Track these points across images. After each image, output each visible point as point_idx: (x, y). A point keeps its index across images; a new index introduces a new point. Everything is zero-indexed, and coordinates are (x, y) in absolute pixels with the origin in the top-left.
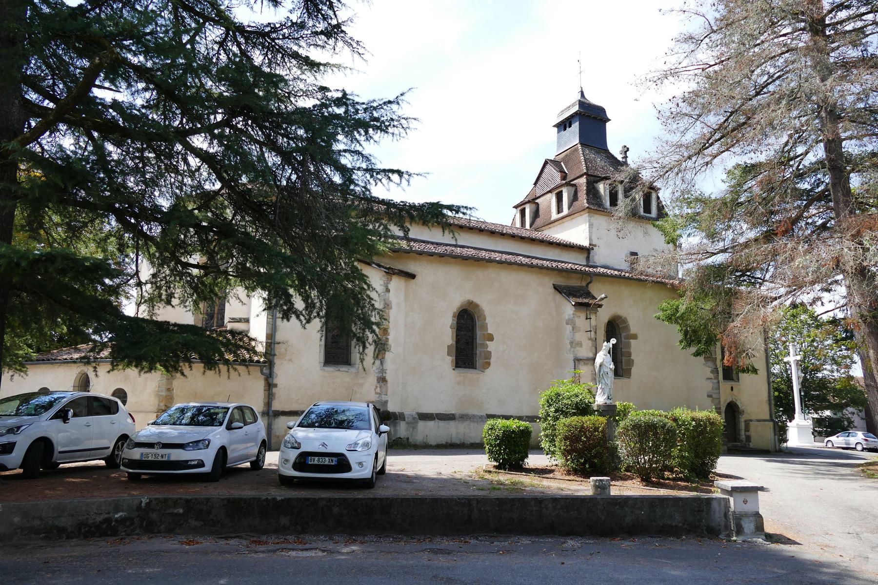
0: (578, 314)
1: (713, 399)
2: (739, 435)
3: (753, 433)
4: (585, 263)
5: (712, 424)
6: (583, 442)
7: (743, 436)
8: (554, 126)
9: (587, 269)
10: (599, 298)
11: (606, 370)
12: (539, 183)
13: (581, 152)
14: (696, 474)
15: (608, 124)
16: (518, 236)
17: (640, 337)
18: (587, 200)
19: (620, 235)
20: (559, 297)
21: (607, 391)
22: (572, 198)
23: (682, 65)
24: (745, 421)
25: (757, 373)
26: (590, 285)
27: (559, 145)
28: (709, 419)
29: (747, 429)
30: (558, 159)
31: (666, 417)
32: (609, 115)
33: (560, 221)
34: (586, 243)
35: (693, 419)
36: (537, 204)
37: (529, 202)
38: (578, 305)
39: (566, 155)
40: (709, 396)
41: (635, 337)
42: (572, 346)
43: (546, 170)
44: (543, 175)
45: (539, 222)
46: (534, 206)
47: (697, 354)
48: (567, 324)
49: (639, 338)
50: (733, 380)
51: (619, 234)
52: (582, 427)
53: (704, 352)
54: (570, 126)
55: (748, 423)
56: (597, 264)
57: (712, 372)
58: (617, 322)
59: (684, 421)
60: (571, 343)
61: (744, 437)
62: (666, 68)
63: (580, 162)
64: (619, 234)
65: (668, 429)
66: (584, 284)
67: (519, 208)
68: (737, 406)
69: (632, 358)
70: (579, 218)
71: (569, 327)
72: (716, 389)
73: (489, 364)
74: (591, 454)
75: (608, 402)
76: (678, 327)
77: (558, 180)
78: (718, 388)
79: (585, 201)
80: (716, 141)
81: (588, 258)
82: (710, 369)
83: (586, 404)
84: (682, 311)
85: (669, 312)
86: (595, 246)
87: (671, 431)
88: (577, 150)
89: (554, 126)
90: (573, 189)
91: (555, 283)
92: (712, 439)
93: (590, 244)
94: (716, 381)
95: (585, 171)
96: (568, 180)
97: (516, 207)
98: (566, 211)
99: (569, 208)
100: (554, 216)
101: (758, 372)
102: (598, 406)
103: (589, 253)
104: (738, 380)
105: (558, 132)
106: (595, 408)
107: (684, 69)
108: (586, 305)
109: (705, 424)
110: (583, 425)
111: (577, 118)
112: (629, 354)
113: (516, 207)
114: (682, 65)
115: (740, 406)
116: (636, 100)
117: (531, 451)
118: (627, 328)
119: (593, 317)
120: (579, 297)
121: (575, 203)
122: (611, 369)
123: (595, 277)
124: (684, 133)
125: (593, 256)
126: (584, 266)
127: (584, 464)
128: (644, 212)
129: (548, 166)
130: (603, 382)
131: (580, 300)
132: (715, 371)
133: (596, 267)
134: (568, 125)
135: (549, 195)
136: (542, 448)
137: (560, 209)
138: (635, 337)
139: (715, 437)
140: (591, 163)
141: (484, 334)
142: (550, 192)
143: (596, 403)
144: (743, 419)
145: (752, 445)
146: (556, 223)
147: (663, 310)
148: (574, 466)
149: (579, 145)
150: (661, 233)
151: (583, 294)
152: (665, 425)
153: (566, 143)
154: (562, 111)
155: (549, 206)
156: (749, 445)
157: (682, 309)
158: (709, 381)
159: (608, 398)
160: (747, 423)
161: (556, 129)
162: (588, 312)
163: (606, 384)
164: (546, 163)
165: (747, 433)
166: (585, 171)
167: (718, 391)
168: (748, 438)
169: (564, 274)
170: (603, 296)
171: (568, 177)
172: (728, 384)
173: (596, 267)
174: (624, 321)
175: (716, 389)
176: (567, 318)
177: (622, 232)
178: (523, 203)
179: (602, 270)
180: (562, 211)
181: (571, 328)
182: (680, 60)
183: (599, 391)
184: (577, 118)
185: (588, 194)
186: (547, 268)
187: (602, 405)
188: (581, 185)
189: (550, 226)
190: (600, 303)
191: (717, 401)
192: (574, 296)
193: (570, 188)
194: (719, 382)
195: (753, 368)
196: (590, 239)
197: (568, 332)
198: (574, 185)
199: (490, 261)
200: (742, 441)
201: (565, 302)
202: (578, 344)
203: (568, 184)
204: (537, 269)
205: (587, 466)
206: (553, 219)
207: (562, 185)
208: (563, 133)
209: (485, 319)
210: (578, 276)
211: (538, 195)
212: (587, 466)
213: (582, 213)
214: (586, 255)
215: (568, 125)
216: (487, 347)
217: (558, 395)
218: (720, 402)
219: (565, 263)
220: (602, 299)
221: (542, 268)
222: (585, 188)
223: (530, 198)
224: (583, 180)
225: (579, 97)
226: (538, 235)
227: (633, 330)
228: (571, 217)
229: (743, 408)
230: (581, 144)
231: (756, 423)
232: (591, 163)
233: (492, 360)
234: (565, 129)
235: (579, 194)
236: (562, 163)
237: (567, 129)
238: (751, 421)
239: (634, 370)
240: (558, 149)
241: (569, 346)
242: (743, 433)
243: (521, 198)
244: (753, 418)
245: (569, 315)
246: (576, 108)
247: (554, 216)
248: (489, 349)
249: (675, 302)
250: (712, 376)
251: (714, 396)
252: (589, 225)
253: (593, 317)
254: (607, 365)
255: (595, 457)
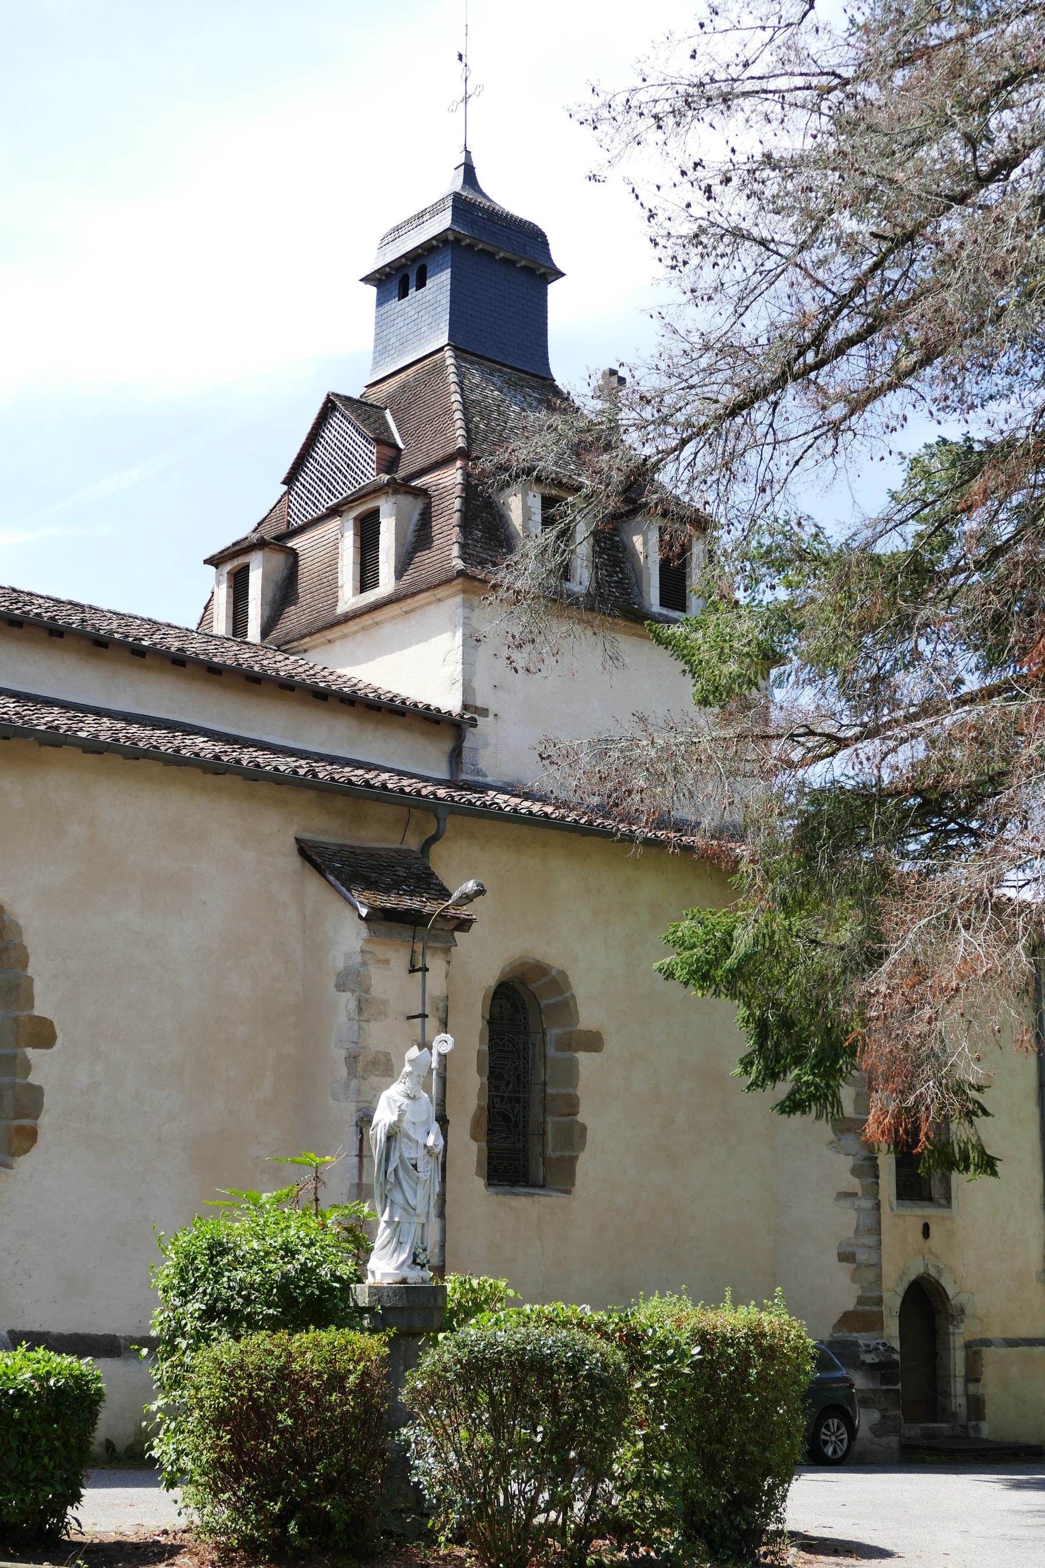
0: (383, 951)
1: (859, 1266)
2: (947, 1394)
3: (990, 1387)
4: (443, 774)
5: (770, 1354)
6: (282, 1432)
7: (959, 1401)
8: (366, 280)
9: (442, 793)
10: (456, 895)
11: (410, 1153)
12: (303, 478)
13: (453, 378)
14: (711, 1544)
15: (554, 289)
16: (122, 644)
17: (612, 1043)
18: (463, 546)
19: (521, 658)
20: (315, 887)
21: (411, 1232)
22: (410, 537)
23: (754, 70)
24: (968, 1346)
25: (994, 1173)
26: (436, 849)
27: (382, 348)
28: (756, 1336)
29: (973, 1375)
30: (375, 397)
31: (600, 1328)
32: (559, 256)
33: (366, 620)
34: (450, 702)
35: (703, 1338)
36: (293, 554)
37: (261, 544)
38: (380, 918)
39: (404, 387)
40: (845, 1257)
41: (593, 1042)
42: (352, 1073)
43: (327, 434)
44: (320, 451)
45: (294, 618)
46: (279, 560)
47: (793, 1105)
48: (341, 987)
49: (607, 1048)
50: (929, 1199)
51: (516, 655)
52: (284, 1373)
53: (812, 1097)
54: (421, 284)
55: (978, 1353)
56: (489, 780)
57: (855, 1171)
58: (533, 987)
59: (663, 1345)
60: (352, 1059)
61: (961, 1401)
62: (696, 71)
63: (448, 412)
64: (516, 655)
65: (590, 1376)
66: (413, 843)
67: (228, 567)
68: (940, 1292)
69: (581, 1118)
70: (433, 609)
71: (346, 1001)
72: (869, 1231)
73: (30, 1136)
74: (309, 1480)
75: (415, 1276)
76: (743, 1012)
77: (370, 474)
78: (876, 1229)
79: (455, 550)
80: (851, 341)
81: (456, 757)
82: (849, 1162)
83: (321, 1285)
84: (742, 950)
85: (699, 951)
86: (484, 712)
87: (603, 1383)
88: (439, 369)
89: (366, 280)
90: (419, 505)
91: (307, 836)
92: (766, 1409)
93: (465, 707)
94: (867, 1204)
95: (461, 443)
96: (401, 474)
97: (215, 561)
98: (387, 583)
99: (399, 574)
100: (348, 599)
101: (999, 1167)
102: (376, 1291)
103: (460, 739)
104: (949, 1199)
105: (381, 301)
106: (363, 1301)
107: (756, 85)
108: (413, 920)
109: (746, 1359)
110: (286, 1366)
111: (447, 256)
112: (572, 1105)
113: (215, 561)
114: (754, 70)
115: (951, 1292)
116: (594, 178)
117: (93, 1473)
118: (567, 1008)
119: (436, 964)
120: (387, 891)
121: (424, 558)
122: (429, 1151)
123: (451, 823)
124: (742, 304)
125: (475, 750)
126: (439, 783)
127: (282, 1520)
128: (662, 604)
129: (336, 420)
130: (398, 1197)
131: (390, 901)
132: (868, 1168)
133: (482, 788)
134: (413, 280)
135: (334, 524)
136: (153, 1461)
137: (367, 578)
138: (593, 1042)
139: (777, 1402)
140: (486, 416)
141: (16, 1019)
142: (335, 512)
143: (370, 1281)
144: (960, 1336)
145: (986, 1430)
146: (352, 626)
147: (681, 944)
148: (247, 1530)
149: (448, 353)
150: (682, 665)
151: (404, 880)
152: (582, 1361)
153: (404, 344)
154: (397, 229)
155: (332, 566)
156: (977, 1429)
157: (743, 941)
158: (846, 1203)
159: (414, 1261)
160: (975, 1349)
161: (372, 291)
162: (419, 947)
163: (409, 1208)
164: (330, 407)
165: (972, 1388)
166: (461, 443)
167: (871, 1240)
168: (976, 1406)
169: (340, 802)
170: (470, 886)
171: (403, 462)
172: (916, 1214)
173: (482, 788)
174: (559, 983)
175: (869, 1231)
176: (340, 965)
177: (528, 647)
178: (241, 549)
179: (501, 799)
180: (375, 584)
181: (352, 1005)
182: (749, 54)
183: (383, 1234)
184: (447, 256)
185: (465, 526)
186: (277, 778)
187: (389, 1288)
188: (445, 492)
189: (330, 634)
190: (464, 912)
191: (870, 1275)
192: (370, 885)
193: (406, 501)
194: (878, 1207)
195: (982, 1153)
196: (467, 689)
197: (342, 1018)
198: (422, 493)
199: (53, 739)
200: (955, 1415)
201: (339, 904)
202: (374, 1063)
203: (402, 487)
204: (156, 767)
205: (293, 1528)
206: (342, 609)
207: (377, 490)
208: (395, 305)
209: (23, 961)
210: (392, 812)
211: (298, 522)
212: (293, 1528)
213: (441, 592)
214: (447, 746)
215: (413, 280)
216: (27, 1067)
217: (217, 1249)
218: (879, 1277)
219: (368, 767)
220: (468, 898)
221: (255, 775)
222: (457, 504)
223: (269, 532)
224: (452, 477)
225: (455, 182)
226: (283, 665)
227: (588, 1017)
228: (407, 604)
229: (962, 1298)
230: (455, 348)
231: (1004, 1351)
232: (486, 416)
233: (45, 1122)
234: (403, 294)
235: (437, 526)
236: (388, 414)
237: (412, 291)
238: (987, 1343)
239: (586, 1165)
240: (376, 364)
241: (343, 1071)
242: (958, 1387)
243: (242, 529)
244: (996, 1333)
245: (348, 956)
246: (443, 221)
247: (348, 599)
248: (33, 1079)
249: (720, 919)
250: (854, 1184)
251: (862, 1256)
252: (466, 637)
253: (436, 964)
254: (417, 1135)
255: (330, 1486)
